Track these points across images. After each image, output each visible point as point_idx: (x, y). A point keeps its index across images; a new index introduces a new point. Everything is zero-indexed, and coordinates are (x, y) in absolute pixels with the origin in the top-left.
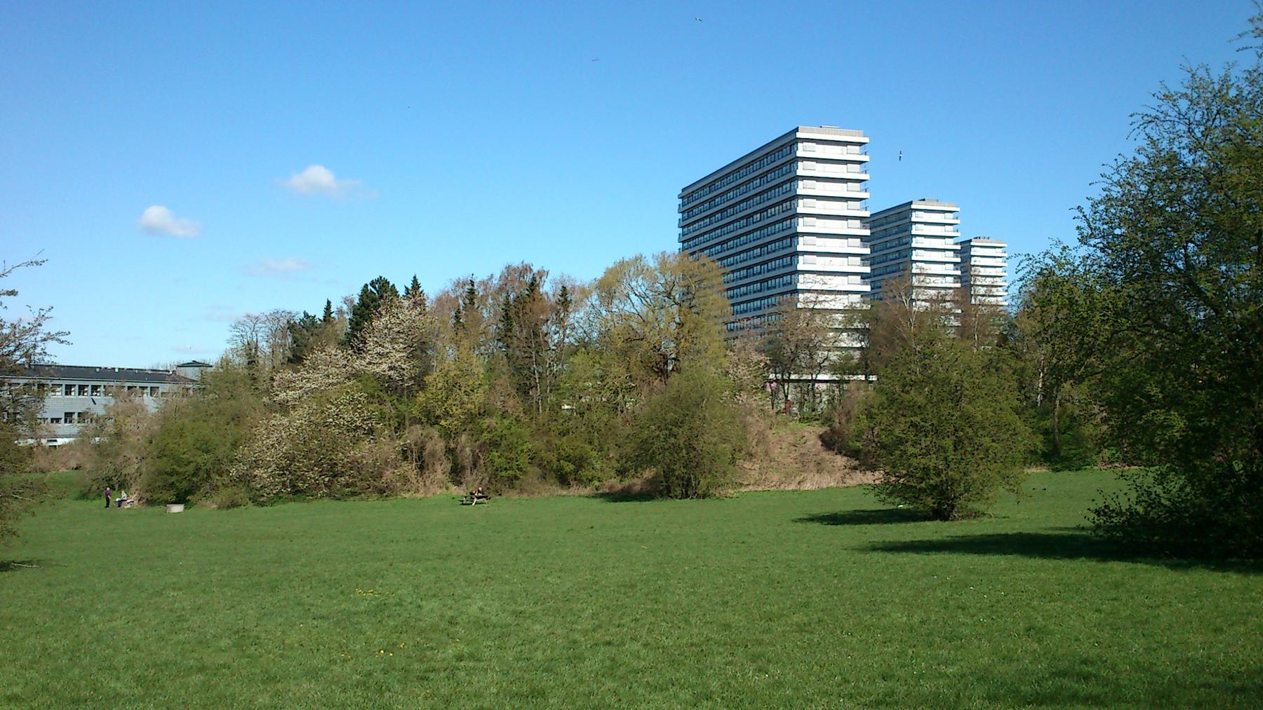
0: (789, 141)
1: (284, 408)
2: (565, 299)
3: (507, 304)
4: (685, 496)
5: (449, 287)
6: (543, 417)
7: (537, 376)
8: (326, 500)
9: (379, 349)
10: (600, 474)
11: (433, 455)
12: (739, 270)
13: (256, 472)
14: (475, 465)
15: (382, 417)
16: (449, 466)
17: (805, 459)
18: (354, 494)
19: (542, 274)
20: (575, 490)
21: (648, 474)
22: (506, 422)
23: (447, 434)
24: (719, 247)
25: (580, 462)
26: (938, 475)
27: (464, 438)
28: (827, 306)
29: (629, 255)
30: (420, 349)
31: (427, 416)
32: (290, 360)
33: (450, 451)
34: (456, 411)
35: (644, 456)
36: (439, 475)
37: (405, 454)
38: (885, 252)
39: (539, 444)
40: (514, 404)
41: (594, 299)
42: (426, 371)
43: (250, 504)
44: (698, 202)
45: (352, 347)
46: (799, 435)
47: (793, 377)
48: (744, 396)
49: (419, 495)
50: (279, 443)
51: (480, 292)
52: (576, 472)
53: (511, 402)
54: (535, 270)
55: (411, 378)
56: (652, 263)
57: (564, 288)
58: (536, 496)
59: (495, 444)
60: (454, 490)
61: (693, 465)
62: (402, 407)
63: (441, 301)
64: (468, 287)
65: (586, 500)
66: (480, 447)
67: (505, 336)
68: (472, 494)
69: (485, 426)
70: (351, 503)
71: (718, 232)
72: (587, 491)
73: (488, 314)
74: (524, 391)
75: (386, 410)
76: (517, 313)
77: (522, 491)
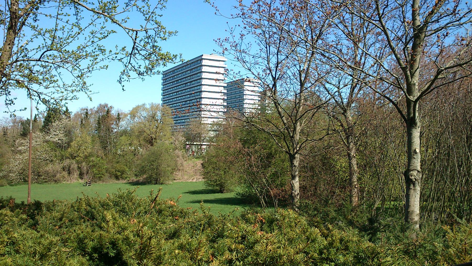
0: (200, 59)
1: (20, 152)
2: (119, 118)
3: (99, 118)
4: (156, 184)
5: (79, 110)
6: (110, 157)
7: (109, 143)
8: (36, 184)
9: (55, 133)
10: (129, 176)
11: (73, 169)
12: (182, 102)
13: (11, 174)
14: (87, 173)
15: (56, 156)
16: (79, 173)
17: (196, 171)
18: (46, 182)
19: (111, 107)
20: (121, 181)
21: (145, 176)
22: (98, 159)
23: (78, 162)
24: (175, 94)
25: (123, 172)
26: (219, 181)
27: (84, 164)
28: (205, 122)
29: (140, 104)
30: (68, 133)
31: (72, 156)
32: (21, 135)
33: (79, 168)
34: (81, 155)
35: (143, 171)
36: (75, 176)
37: (64, 169)
38: (235, 95)
39: (109, 166)
40: (101, 153)
41: (129, 117)
42: (71, 141)
43: (8, 186)
44: (168, 77)
45: (45, 132)
46: (195, 163)
47: (195, 143)
48: (177, 150)
49: (69, 183)
50: (19, 165)
51: (90, 113)
52: (121, 175)
53: (100, 152)
54: (109, 106)
55: (65, 143)
56: (148, 106)
57: (119, 114)
58: (108, 183)
59: (94, 166)
60: (80, 181)
61: (158, 174)
62: (63, 153)
63: (77, 115)
64: (86, 111)
65: (124, 184)
66: (89, 167)
67: (98, 128)
68: (87, 182)
69: (91, 160)
70: (45, 185)
71: (175, 88)
72: (125, 181)
73: (93, 120)
74: (105, 148)
75: (57, 154)
76: (102, 121)
77: (103, 181)
